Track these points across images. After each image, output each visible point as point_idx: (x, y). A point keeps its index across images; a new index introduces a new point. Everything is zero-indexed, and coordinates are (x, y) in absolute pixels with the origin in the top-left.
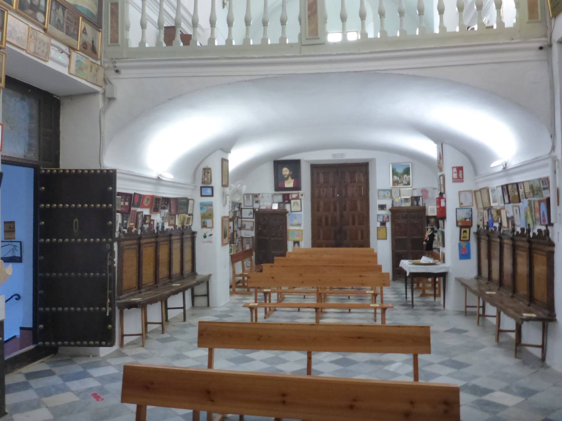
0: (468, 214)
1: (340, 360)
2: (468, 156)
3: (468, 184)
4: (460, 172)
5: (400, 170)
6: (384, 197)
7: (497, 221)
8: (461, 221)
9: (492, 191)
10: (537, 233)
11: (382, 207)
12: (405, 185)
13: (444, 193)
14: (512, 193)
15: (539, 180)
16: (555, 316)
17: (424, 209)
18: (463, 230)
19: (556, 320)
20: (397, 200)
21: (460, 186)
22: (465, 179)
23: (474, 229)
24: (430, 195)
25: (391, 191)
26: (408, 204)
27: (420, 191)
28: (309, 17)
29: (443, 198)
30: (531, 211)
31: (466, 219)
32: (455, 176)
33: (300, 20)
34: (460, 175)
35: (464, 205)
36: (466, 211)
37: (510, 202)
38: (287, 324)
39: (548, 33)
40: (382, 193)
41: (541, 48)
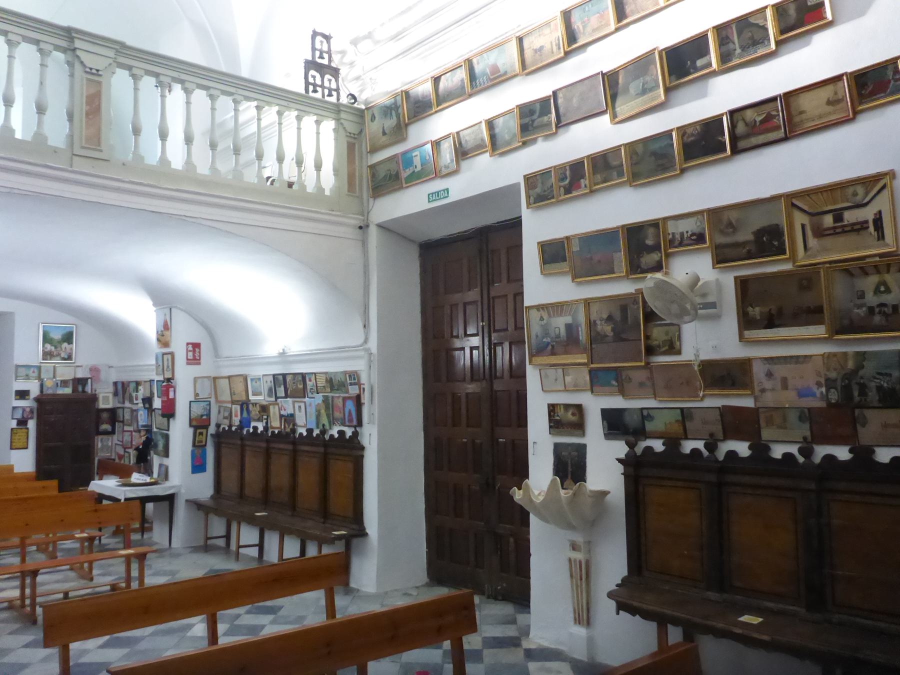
0: (205, 409)
1: (108, 641)
2: (204, 328)
3: (206, 368)
4: (197, 350)
5: (56, 336)
6: (27, 377)
7: (259, 420)
8: (196, 419)
9: (252, 380)
10: (336, 436)
11: (22, 394)
12: (64, 359)
13: (173, 378)
14: (291, 385)
15: (345, 373)
16: (364, 529)
17: (94, 398)
18: (199, 431)
19: (367, 534)
20: (49, 383)
21: (195, 371)
22: (202, 361)
23: (212, 430)
24: (103, 376)
25: (39, 368)
26: (68, 391)
27: (88, 370)
28: (87, 114)
29: (172, 387)
30: (327, 408)
31: (202, 416)
32: (190, 355)
33: (70, 117)
34: (197, 354)
35: (201, 397)
36: (203, 404)
37: (286, 396)
38: (240, 571)
39: (365, 212)
40: (22, 372)
41: (361, 228)
